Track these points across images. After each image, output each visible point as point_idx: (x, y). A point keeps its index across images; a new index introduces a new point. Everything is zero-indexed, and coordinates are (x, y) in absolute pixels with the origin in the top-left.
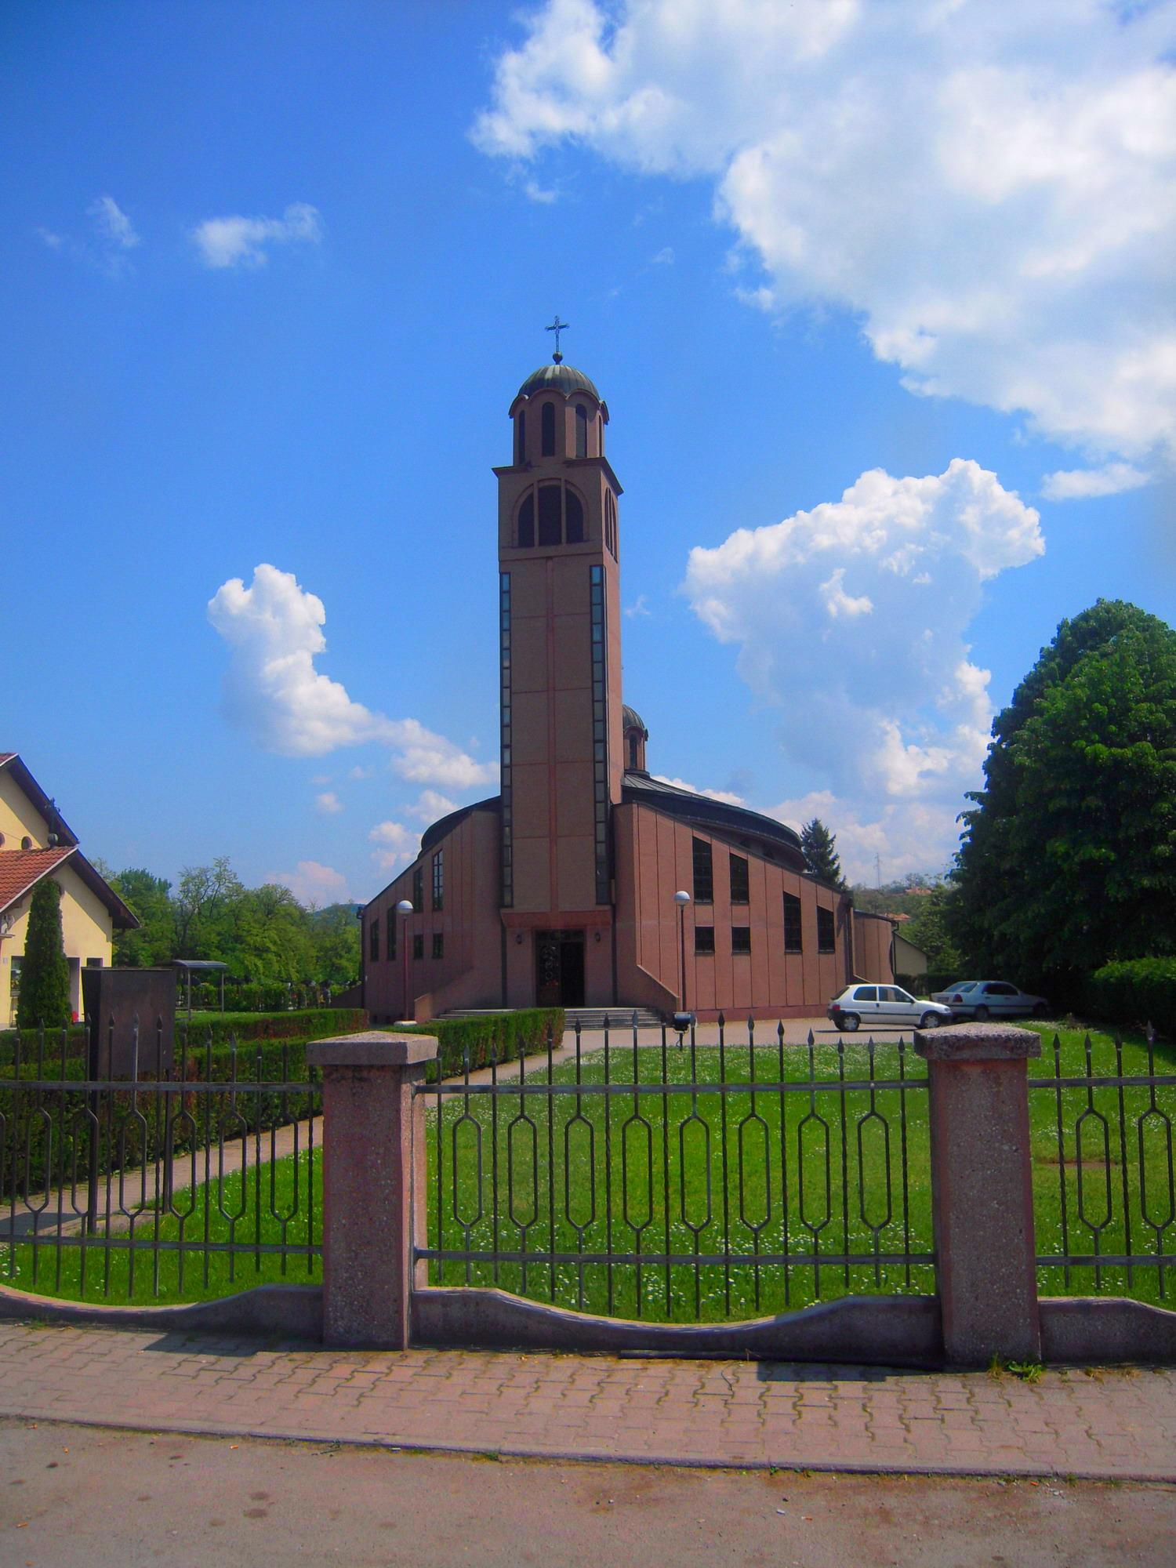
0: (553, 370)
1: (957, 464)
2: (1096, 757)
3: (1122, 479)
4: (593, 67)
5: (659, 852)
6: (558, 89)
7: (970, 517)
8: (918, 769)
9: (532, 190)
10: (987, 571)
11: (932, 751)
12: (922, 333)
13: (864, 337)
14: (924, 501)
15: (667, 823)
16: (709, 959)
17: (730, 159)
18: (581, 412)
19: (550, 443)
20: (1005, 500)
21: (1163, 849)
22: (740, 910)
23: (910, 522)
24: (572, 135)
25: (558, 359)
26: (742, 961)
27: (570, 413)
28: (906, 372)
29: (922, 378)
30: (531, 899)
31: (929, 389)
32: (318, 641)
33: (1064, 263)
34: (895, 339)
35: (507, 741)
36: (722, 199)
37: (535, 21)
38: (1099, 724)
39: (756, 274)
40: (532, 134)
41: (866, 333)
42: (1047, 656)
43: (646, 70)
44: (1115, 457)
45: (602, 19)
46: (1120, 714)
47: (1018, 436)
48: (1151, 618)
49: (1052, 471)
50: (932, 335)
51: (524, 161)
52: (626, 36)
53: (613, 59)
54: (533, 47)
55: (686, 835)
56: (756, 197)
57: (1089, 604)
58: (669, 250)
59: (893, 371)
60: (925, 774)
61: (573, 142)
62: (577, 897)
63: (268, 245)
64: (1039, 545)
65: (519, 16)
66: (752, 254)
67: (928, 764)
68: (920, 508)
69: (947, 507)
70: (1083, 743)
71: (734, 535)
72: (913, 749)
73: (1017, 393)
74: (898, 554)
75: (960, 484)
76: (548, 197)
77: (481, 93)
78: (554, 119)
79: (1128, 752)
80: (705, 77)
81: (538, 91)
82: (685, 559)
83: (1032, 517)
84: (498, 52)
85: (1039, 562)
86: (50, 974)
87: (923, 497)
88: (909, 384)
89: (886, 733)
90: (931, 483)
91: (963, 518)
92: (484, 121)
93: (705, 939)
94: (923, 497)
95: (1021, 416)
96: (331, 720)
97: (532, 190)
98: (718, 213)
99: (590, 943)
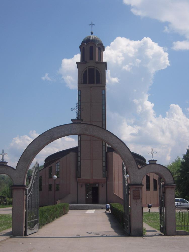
0: (92, 37)
5: (117, 161)
7: (149, 53)
19: (92, 57)
23: (131, 55)
27: (97, 49)
28: (133, 7)
30: (85, 175)
31: (139, 13)
60: (132, 134)
62: (98, 175)
64: (168, 62)
69: (141, 50)
72: (130, 127)
74: (127, 66)
75: (145, 43)
83: (166, 55)
90: (137, 42)
95: (167, 24)
99: (100, 186)
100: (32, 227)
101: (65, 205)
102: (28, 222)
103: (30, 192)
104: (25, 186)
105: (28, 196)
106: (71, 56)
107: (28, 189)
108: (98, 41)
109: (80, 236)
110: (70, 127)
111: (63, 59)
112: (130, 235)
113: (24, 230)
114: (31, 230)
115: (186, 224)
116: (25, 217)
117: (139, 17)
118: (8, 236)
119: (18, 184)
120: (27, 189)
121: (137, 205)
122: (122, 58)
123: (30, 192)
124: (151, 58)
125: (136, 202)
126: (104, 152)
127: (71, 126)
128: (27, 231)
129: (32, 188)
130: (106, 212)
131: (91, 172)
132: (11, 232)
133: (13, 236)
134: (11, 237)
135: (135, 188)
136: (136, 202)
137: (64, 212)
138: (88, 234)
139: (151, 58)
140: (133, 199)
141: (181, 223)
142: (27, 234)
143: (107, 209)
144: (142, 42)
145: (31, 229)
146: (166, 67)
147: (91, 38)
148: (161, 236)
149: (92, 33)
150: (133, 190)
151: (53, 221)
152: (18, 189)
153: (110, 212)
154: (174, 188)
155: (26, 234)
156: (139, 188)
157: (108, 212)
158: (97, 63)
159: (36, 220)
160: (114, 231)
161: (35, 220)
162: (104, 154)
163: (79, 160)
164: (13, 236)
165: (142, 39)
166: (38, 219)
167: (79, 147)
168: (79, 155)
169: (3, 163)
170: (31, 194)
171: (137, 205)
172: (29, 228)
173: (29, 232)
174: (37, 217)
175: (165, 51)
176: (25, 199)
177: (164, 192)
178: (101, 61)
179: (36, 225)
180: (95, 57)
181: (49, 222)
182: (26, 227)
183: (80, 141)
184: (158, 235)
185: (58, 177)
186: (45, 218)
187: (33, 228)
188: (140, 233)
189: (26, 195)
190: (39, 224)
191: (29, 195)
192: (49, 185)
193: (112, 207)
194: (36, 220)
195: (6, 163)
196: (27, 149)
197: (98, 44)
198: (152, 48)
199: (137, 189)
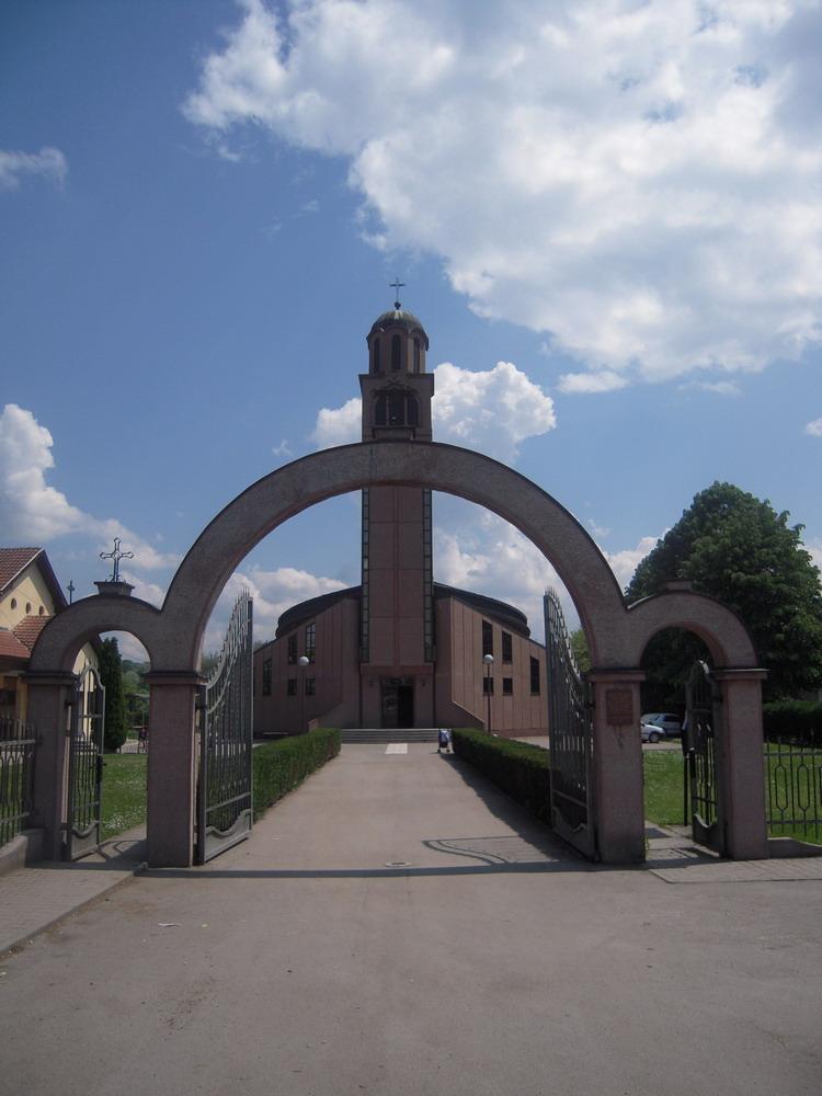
0: (398, 313)
1: (502, 365)
2: (738, 579)
3: (609, 382)
4: (272, 72)
5: (465, 627)
6: (246, 83)
7: (510, 400)
8: (468, 570)
9: (223, 151)
10: (518, 437)
11: (478, 557)
12: (484, 274)
13: (446, 274)
14: (478, 388)
15: (468, 610)
16: (510, 698)
17: (363, 145)
18: (416, 342)
19: (398, 360)
20: (530, 389)
21: (781, 636)
22: (507, 667)
23: (470, 402)
24: (254, 116)
25: (398, 306)
26: (508, 699)
27: (411, 342)
28: (473, 300)
29: (483, 304)
30: (381, 657)
31: (487, 312)
32: (47, 460)
33: (577, 238)
34: (467, 278)
35: (428, 560)
36: (354, 170)
37: (233, 36)
38: (737, 558)
39: (375, 224)
40: (226, 113)
41: (449, 273)
42: (688, 516)
43: (308, 78)
44: (605, 368)
45: (280, 41)
46: (749, 554)
47: (545, 347)
48: (749, 495)
49: (565, 373)
50: (492, 277)
51: (219, 130)
52: (296, 55)
53: (287, 69)
54: (232, 54)
55: (479, 618)
56: (378, 171)
57: (708, 485)
58: (315, 202)
59: (464, 299)
60: (471, 573)
61: (257, 123)
62: (412, 656)
63: (19, 173)
64: (551, 420)
65: (223, 31)
66: (374, 212)
67: (475, 567)
68: (476, 392)
69: (494, 392)
70: (730, 571)
71: (349, 402)
72: (466, 556)
73: (546, 319)
74: (461, 423)
75: (502, 377)
76: (234, 157)
77: (193, 80)
78: (243, 105)
79: (758, 578)
80: (350, 88)
81: (233, 84)
82: (316, 416)
83: (548, 403)
84: (207, 55)
85: (552, 431)
86: (116, 703)
87: (478, 385)
88: (475, 308)
89: (447, 543)
90: (483, 376)
91: (505, 400)
92: (194, 100)
93: (488, 685)
94: (478, 385)
95: (547, 336)
96: (55, 519)
97: (223, 151)
98: (352, 180)
99: (418, 686)
100: (223, 826)
101: (332, 734)
102: (210, 809)
103: (220, 699)
104: (195, 675)
105: (208, 712)
106: (336, 405)
107: (209, 685)
108: (415, 324)
109: (408, 864)
110: (368, 453)
111: (321, 409)
112: (597, 859)
113: (193, 841)
114: (222, 837)
115: (810, 814)
116: (198, 794)
117: (487, 320)
118: (126, 870)
119: (171, 669)
120: (205, 687)
121: (621, 745)
122: (451, 408)
123: (220, 699)
124: (514, 409)
125: (621, 735)
126: (428, 600)
127: (371, 451)
128: (203, 847)
129: (227, 683)
130: (439, 751)
131: (396, 649)
132: (141, 842)
133: (151, 865)
134: (137, 874)
135: (615, 682)
136: (621, 735)
137: (328, 752)
138: (427, 849)
139: (514, 409)
140: (609, 723)
141: (782, 811)
142: (203, 858)
143: (443, 745)
144: (494, 371)
145: (221, 833)
146: (548, 429)
147: (396, 317)
148: (711, 865)
149: (398, 306)
150: (608, 692)
151: (302, 783)
152: (694, 775)
153: (452, 752)
154: (755, 680)
155: (199, 860)
156: (629, 682)
157: (444, 750)
158: (411, 376)
159: (242, 796)
160: (515, 834)
161: (237, 798)
162: (428, 604)
163: (365, 618)
164: (151, 865)
165: (495, 366)
166: (248, 794)
167: (366, 586)
168: (365, 606)
169: (114, 589)
170: (220, 704)
171: (621, 745)
172: (213, 833)
173: (212, 847)
174: (246, 788)
175: (546, 395)
176: (198, 724)
177: (70, 708)
178: (421, 372)
179: (241, 818)
180: (407, 360)
181: (289, 790)
182: (198, 829)
183: (368, 570)
184: (694, 855)
185: (311, 662)
186: (274, 782)
187: (231, 830)
188: (634, 858)
189: (202, 707)
190: (251, 810)
191: (213, 708)
192: (289, 681)
193: (455, 738)
194: (242, 796)
195: (130, 588)
196: (205, 536)
197: (414, 331)
198: (517, 388)
199: (621, 687)
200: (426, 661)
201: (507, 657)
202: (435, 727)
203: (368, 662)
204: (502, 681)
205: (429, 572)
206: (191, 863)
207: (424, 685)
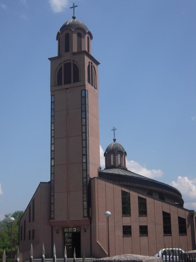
15: (110, 185)
18: (80, 36)
30: (60, 216)
158: (74, 54)
178: (83, 50)
200: (84, 217)
201: (143, 211)
202: (91, 258)
203: (54, 219)
204: (138, 228)
205: (52, 108)
206: (63, 83)
207: (85, 231)
